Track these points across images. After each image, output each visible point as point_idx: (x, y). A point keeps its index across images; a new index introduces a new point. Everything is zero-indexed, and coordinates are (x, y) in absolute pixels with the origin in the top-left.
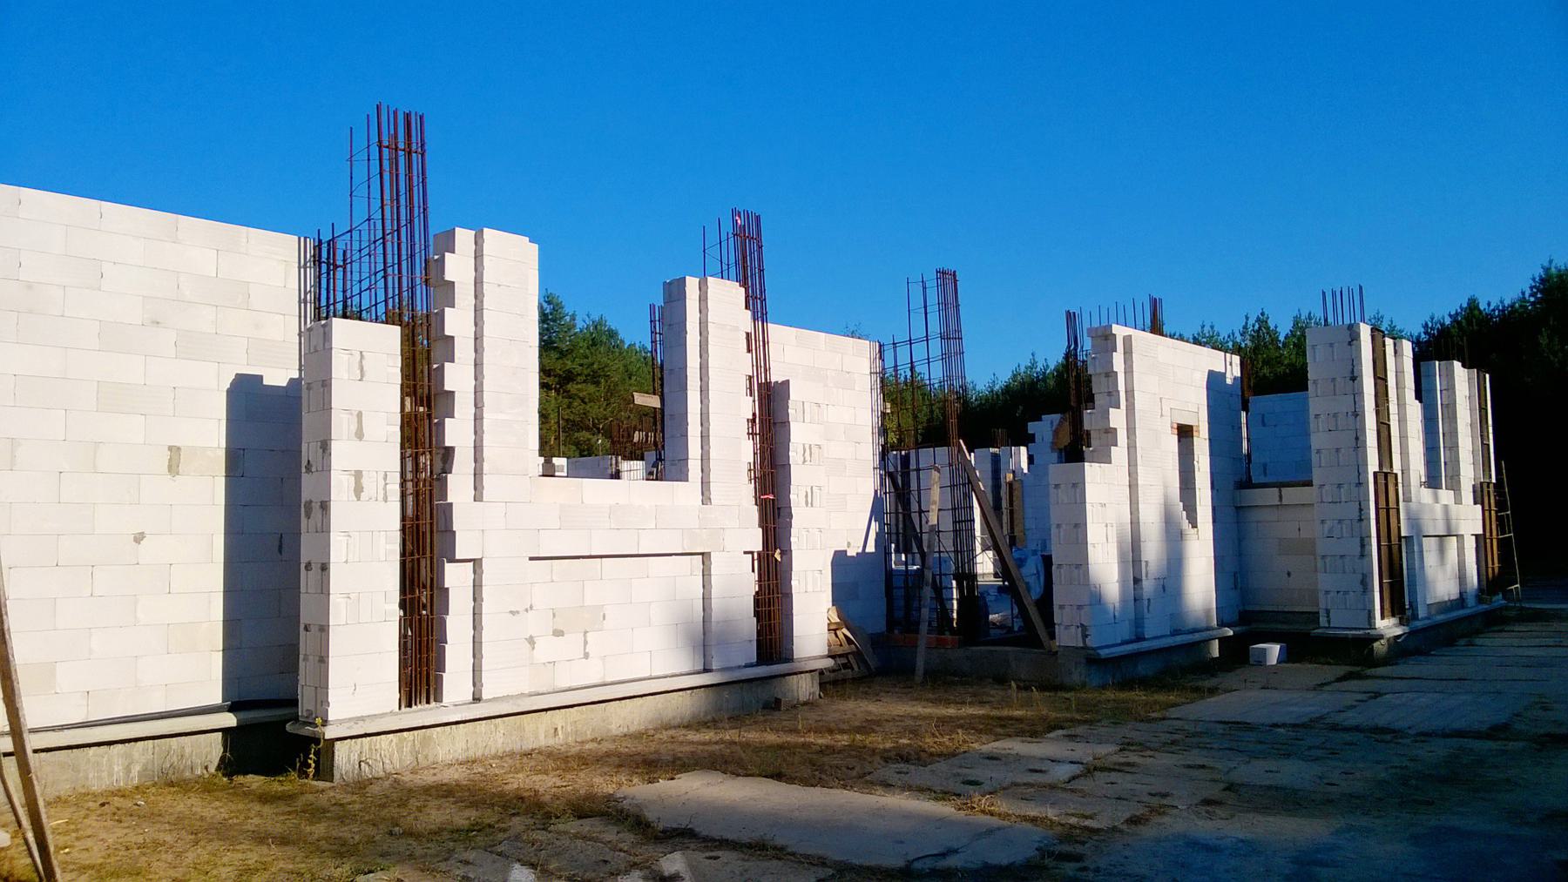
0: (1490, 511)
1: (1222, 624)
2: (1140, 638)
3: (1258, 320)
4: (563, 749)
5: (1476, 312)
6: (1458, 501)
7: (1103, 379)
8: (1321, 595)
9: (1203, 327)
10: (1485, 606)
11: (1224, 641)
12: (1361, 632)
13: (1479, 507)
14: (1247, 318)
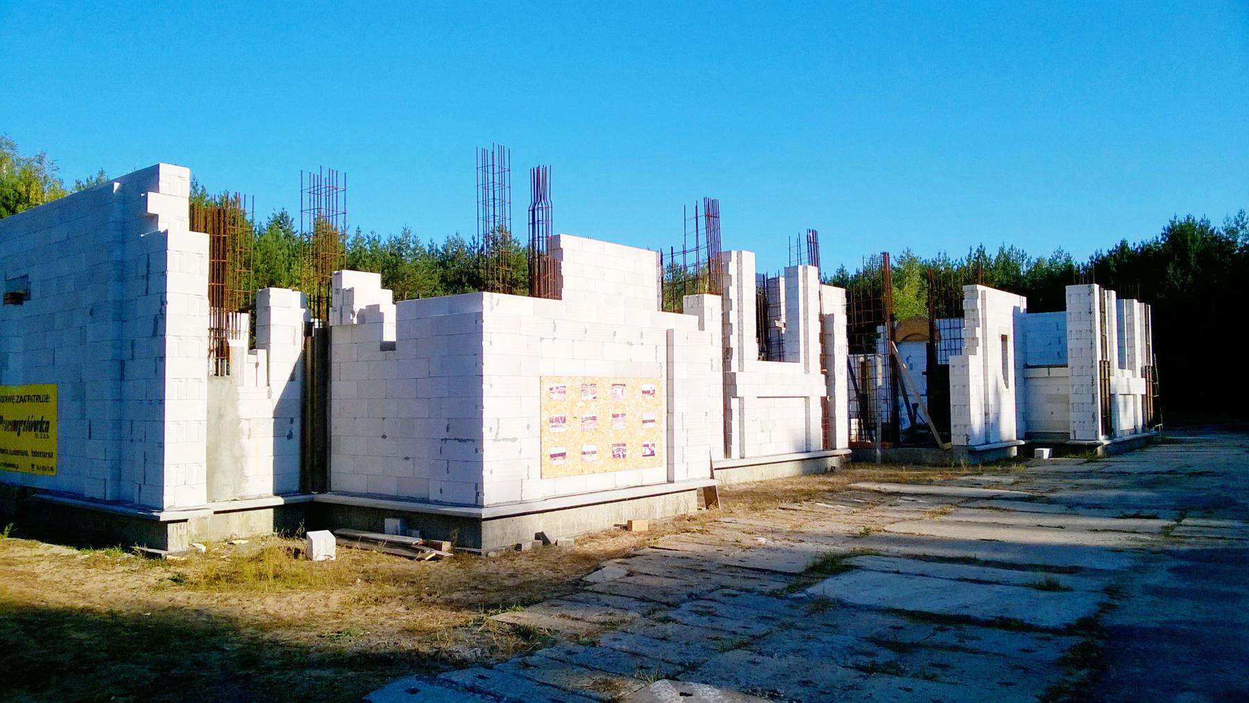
0: (1149, 382)
1: (1018, 438)
2: (987, 443)
3: (978, 251)
4: (857, 466)
5: (1126, 250)
6: (1134, 376)
7: (971, 312)
8: (1071, 424)
9: (939, 254)
10: (1147, 434)
11: (1019, 447)
12: (1092, 442)
13: (1144, 379)
14: (971, 249)
